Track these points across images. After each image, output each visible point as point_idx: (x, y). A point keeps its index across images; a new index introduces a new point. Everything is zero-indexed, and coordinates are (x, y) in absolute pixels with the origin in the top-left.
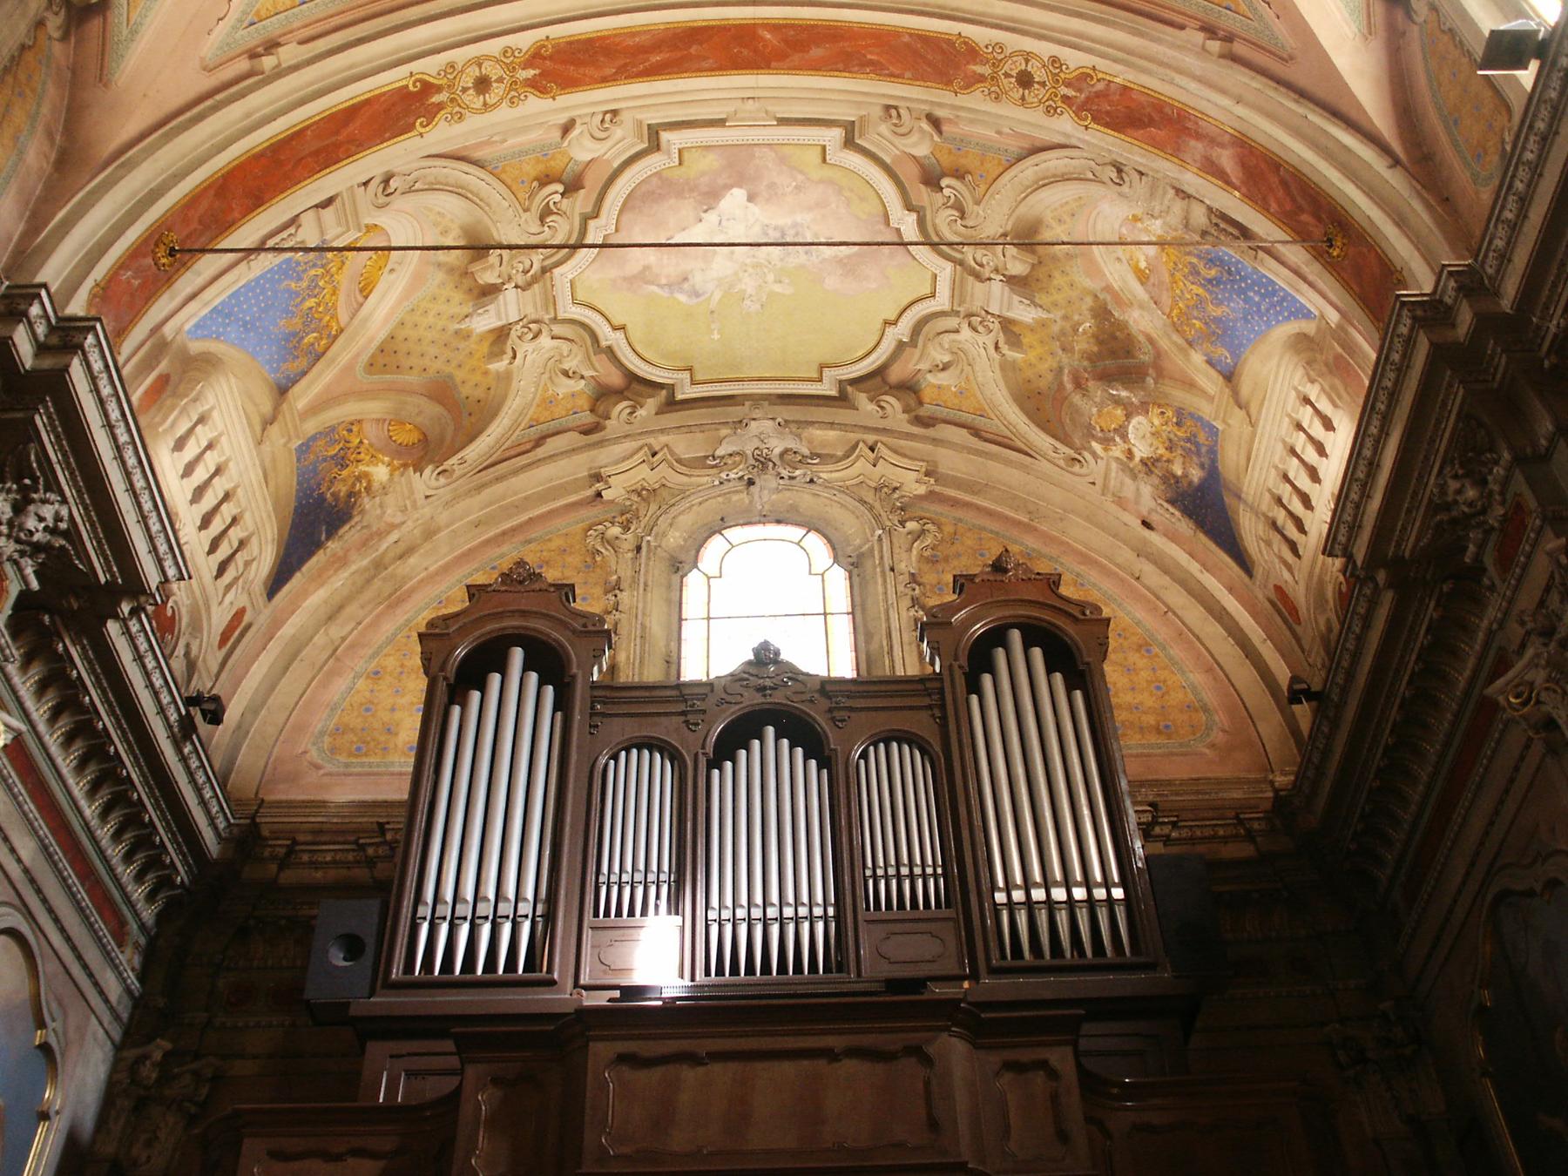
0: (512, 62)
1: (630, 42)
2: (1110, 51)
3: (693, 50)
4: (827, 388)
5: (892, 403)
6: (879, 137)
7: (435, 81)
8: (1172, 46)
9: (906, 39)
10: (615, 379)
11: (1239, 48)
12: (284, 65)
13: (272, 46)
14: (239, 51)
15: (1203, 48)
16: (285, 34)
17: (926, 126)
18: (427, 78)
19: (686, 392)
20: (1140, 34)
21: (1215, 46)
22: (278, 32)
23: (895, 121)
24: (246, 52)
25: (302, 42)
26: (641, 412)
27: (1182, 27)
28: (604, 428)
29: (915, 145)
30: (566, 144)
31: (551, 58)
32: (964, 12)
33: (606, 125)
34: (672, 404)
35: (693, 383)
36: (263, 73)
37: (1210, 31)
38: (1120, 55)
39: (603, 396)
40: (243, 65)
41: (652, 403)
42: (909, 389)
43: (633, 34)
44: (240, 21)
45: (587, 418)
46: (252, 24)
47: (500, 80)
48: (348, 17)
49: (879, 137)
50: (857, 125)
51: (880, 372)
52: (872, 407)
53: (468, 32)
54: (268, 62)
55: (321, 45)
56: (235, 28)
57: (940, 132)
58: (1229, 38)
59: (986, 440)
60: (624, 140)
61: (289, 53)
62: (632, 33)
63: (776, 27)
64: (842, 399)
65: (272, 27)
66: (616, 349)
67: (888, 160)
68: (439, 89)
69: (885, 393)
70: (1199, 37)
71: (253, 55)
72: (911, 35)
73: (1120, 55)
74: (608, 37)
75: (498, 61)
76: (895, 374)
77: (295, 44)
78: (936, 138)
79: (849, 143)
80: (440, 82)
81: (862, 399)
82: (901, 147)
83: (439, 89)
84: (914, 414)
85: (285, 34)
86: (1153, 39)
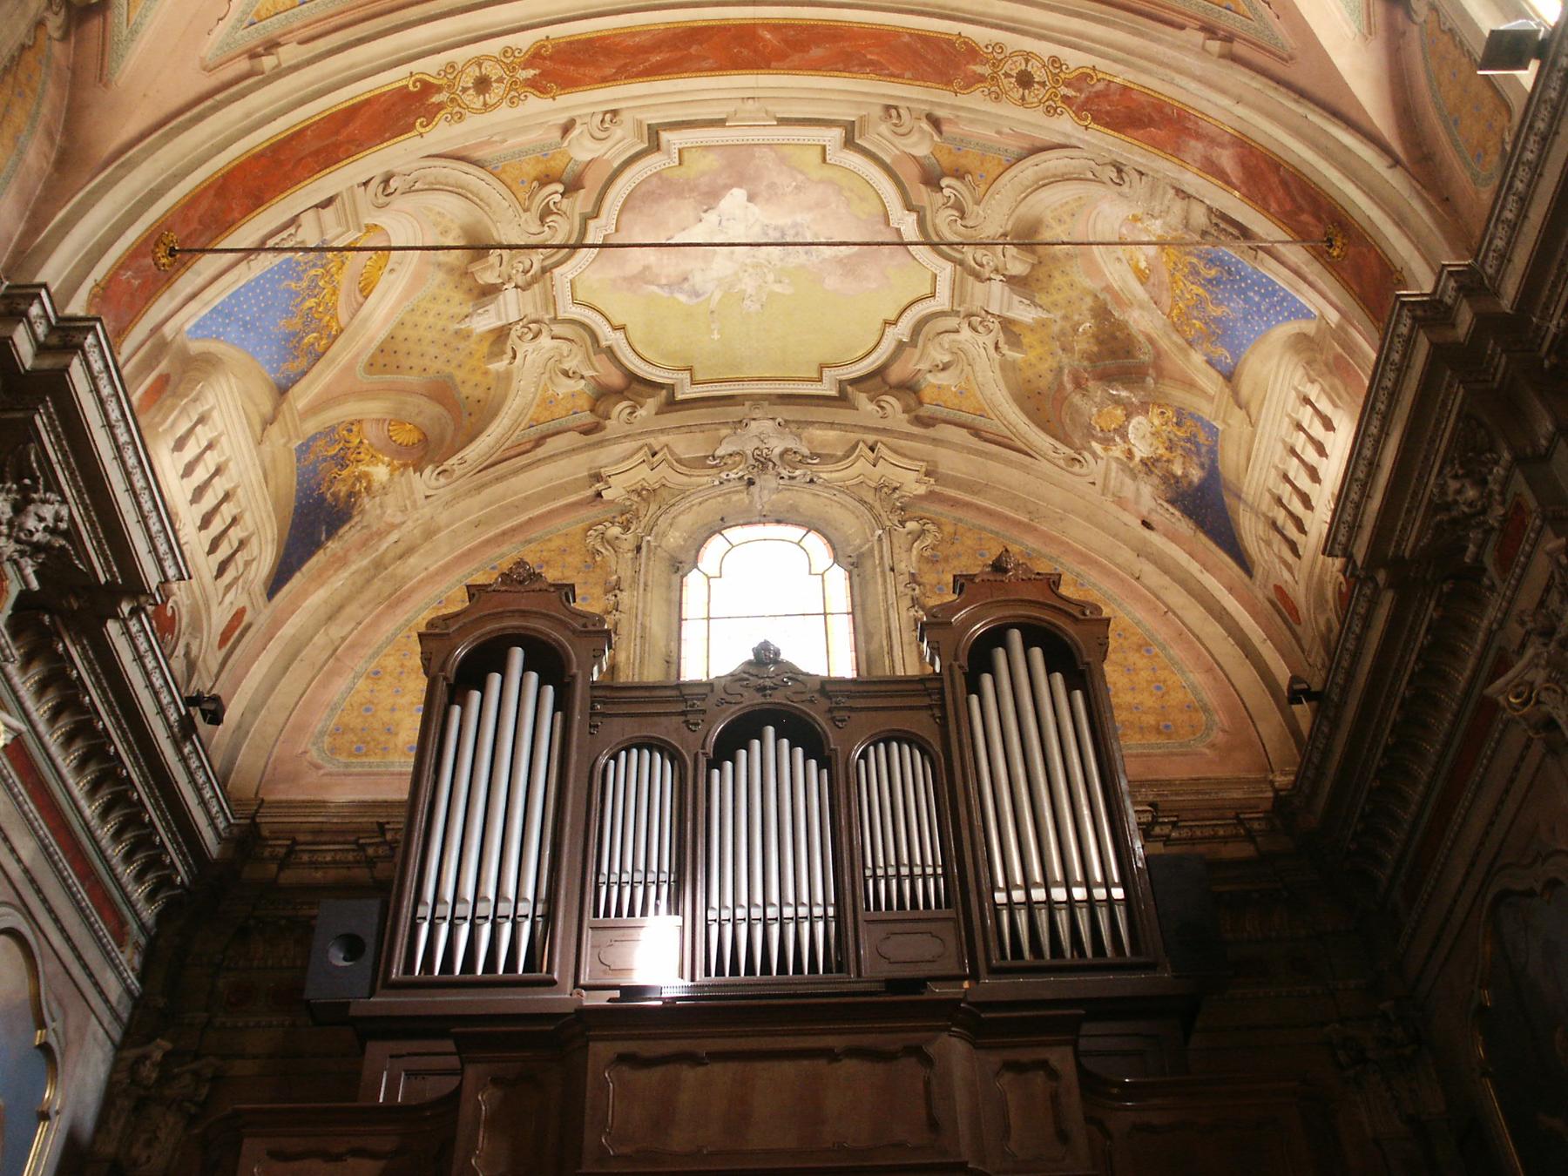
0: (512, 62)
1: (630, 42)
2: (1110, 51)
3: (693, 50)
4: (827, 388)
5: (892, 403)
6: (879, 137)
7: (435, 81)
8: (1172, 46)
9: (906, 39)
10: (615, 379)
11: (1239, 48)
12: (284, 65)
13: (272, 46)
14: (239, 51)
15: (1203, 48)
16: (285, 34)
17: (926, 126)
18: (427, 78)
19: (686, 392)
20: (1140, 34)
21: (1215, 46)
22: (278, 32)
23: (895, 121)
24: (246, 52)
25: (302, 42)
26: (641, 412)
27: (1182, 27)
28: (604, 428)
29: (915, 145)
30: (566, 144)
31: (551, 58)
32: (964, 12)
33: (606, 125)
34: (672, 404)
35: (693, 383)
36: (263, 73)
37: (1210, 31)
38: (1120, 55)
39: (603, 396)
40: (243, 65)
41: (652, 403)
42: (909, 389)
43: (633, 34)
44: (240, 21)
45: (587, 418)
46: (252, 24)
47: (500, 80)
48: (348, 17)
49: (879, 137)
50: (857, 125)
51: (880, 372)
52: (872, 407)
53: (468, 32)
54: (268, 62)
55: (321, 45)
56: (235, 28)
57: (940, 132)
58: (1229, 38)
59: (986, 440)
60: (624, 140)
61: (289, 53)
62: (632, 33)
63: (776, 27)
64: (842, 399)
65: (272, 27)
66: (616, 349)
67: (888, 160)
68: (439, 89)
69: (885, 393)
70: (1199, 37)
71: (253, 55)
72: (911, 35)
73: (1120, 55)
74: (608, 37)
75: (498, 61)
76: (895, 374)
77: (295, 44)
78: (936, 138)
79: (849, 143)
80: (440, 82)
81: (862, 399)
82: (901, 147)
83: (439, 89)
84: (914, 414)
85: (285, 34)
86: (1153, 39)
